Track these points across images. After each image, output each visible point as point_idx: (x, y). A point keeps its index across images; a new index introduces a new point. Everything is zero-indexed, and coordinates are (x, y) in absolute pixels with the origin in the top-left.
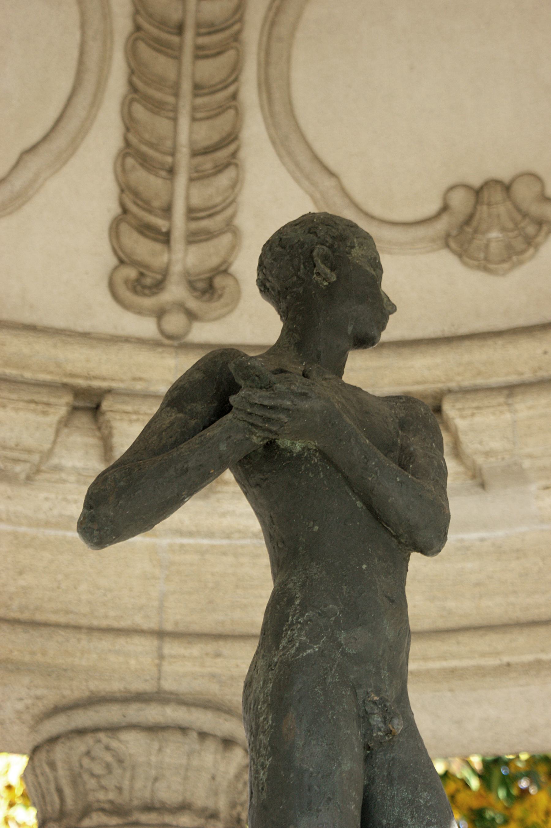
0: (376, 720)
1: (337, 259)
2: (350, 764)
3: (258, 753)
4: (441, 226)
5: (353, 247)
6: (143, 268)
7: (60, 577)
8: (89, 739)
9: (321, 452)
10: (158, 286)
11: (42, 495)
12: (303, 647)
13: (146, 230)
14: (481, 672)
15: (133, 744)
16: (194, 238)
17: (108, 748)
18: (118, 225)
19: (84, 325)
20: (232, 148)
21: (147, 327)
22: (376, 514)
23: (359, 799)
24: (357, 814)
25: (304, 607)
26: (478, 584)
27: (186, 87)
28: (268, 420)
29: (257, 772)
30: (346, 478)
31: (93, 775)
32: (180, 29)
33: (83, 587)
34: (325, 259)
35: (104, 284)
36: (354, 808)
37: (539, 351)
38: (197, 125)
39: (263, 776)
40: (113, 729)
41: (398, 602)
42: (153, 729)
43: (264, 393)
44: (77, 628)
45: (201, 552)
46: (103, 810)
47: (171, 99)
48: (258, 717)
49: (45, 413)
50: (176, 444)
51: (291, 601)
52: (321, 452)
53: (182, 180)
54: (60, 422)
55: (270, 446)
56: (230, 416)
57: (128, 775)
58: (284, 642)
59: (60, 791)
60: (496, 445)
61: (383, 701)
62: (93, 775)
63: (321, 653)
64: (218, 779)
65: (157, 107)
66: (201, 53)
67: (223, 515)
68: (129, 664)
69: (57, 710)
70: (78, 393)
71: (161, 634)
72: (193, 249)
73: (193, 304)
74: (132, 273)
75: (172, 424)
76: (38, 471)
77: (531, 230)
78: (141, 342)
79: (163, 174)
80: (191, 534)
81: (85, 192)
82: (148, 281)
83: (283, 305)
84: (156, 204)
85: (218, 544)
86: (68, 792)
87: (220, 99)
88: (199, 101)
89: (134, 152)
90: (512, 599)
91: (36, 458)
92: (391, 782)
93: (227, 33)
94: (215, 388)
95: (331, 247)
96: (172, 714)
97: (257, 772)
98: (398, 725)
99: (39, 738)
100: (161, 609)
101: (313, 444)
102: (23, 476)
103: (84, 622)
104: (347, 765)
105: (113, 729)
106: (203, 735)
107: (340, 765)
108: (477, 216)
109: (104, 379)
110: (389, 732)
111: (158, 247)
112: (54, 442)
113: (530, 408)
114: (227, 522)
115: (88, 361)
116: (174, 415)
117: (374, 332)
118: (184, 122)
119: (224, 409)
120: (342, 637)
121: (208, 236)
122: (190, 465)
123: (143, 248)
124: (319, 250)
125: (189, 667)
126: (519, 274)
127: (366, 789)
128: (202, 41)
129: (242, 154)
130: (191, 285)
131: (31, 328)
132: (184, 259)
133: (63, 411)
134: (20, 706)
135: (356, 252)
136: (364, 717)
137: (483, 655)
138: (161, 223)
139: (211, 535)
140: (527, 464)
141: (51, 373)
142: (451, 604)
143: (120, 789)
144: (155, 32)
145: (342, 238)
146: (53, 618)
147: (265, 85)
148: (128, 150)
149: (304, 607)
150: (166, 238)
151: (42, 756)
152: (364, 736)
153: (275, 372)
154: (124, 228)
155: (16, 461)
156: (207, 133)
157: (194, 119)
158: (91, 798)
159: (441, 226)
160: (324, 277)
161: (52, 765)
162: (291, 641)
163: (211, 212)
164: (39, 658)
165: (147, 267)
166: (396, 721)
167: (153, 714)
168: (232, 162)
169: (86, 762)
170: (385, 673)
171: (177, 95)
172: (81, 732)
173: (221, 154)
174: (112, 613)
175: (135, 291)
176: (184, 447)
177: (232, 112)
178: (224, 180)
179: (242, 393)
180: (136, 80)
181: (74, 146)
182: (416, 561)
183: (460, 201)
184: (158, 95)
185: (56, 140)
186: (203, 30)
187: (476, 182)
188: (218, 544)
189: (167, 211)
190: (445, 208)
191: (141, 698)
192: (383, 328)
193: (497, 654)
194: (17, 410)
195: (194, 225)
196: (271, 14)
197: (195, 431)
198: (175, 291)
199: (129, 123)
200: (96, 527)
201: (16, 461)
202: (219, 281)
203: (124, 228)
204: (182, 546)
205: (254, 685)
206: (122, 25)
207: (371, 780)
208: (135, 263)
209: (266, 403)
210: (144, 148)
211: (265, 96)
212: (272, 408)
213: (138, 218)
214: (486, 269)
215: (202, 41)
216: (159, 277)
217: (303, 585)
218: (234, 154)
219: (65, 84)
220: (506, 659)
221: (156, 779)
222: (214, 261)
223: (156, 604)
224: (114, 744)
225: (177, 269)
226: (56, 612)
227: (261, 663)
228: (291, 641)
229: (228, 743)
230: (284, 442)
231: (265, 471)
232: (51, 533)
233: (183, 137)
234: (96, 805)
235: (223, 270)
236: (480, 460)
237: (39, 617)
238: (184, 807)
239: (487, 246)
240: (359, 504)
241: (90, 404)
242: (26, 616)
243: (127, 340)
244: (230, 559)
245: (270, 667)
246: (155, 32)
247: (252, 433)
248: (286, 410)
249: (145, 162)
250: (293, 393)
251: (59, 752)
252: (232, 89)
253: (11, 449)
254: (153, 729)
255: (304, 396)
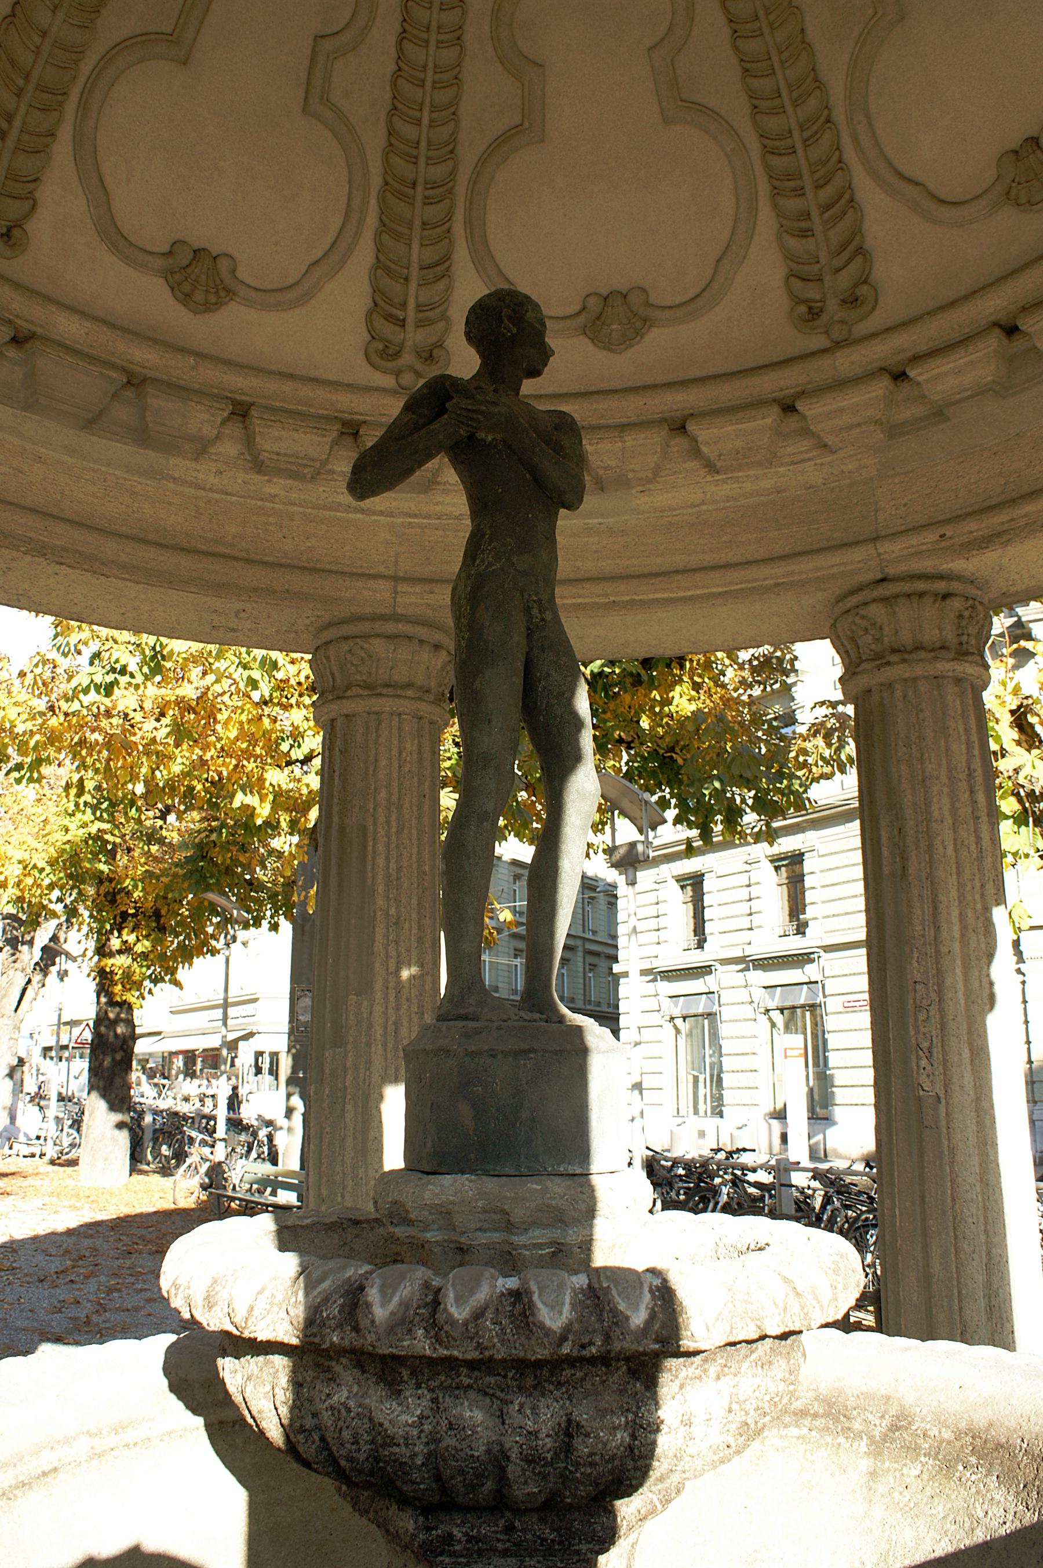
0: (535, 612)
1: (518, 319)
2: (518, 638)
3: (461, 631)
4: (581, 320)
5: (527, 311)
6: (387, 343)
7: (332, 541)
8: (351, 642)
9: (505, 441)
10: (397, 355)
11: (321, 489)
12: (490, 565)
13: (389, 318)
14: (597, 606)
15: (378, 646)
16: (420, 324)
17: (362, 648)
18: (400, 44)
19: (350, 379)
20: (447, 264)
21: (389, 381)
22: (539, 482)
23: (523, 659)
24: (522, 668)
25: (491, 540)
26: (596, 552)
27: (417, 223)
28: (471, 419)
29: (459, 641)
30: (520, 459)
31: (353, 665)
32: (414, 185)
33: (347, 548)
34: (510, 318)
35: (362, 353)
36: (520, 665)
37: (641, 403)
38: (423, 248)
39: (463, 644)
40: (366, 637)
41: (551, 540)
42: (389, 637)
43: (469, 401)
44: (344, 573)
45: (422, 527)
46: (359, 686)
47: (407, 232)
48: (460, 608)
49: (324, 436)
50: (411, 434)
51: (483, 535)
52: (505, 441)
53: (413, 285)
54: (333, 441)
55: (472, 437)
56: (446, 416)
57: (375, 664)
58: (478, 562)
59: (332, 674)
60: (612, 463)
61: (540, 600)
62: (353, 665)
63: (502, 569)
64: (431, 669)
65: (397, 236)
66: (427, 202)
67: (436, 504)
68: (376, 596)
69: (330, 625)
70: (345, 423)
71: (396, 579)
72: (420, 330)
73: (419, 367)
74: (381, 346)
75: (408, 421)
76: (319, 473)
77: (639, 324)
78: (385, 390)
79: (402, 281)
80: (415, 516)
81: (350, 292)
82: (390, 352)
83: (481, 348)
84: (396, 301)
85: (438, 506)
86: (337, 674)
87: (439, 231)
88: (426, 233)
89: (381, 267)
90: (618, 561)
91: (318, 464)
92: (543, 651)
93: (445, 188)
94: (435, 400)
95: (513, 310)
96: (402, 628)
97: (459, 641)
98: (548, 615)
99: (319, 642)
100: (396, 562)
101: (499, 436)
102: (309, 476)
103: (348, 570)
104: (516, 638)
105: (366, 637)
106: (421, 641)
107: (512, 638)
108: (604, 315)
109: (362, 415)
110: (543, 620)
111: (398, 329)
112: (329, 454)
113: (634, 440)
114: (438, 508)
115: (351, 402)
116: (410, 416)
117: (540, 367)
118: (416, 246)
119: (443, 411)
120: (515, 559)
121: (430, 322)
122: (420, 447)
123: (387, 330)
124: (506, 312)
125: (414, 599)
126: (629, 354)
127: (528, 654)
128: (427, 193)
129: (453, 269)
130: (418, 355)
131: (315, 380)
132: (414, 337)
133: (335, 434)
134: (307, 622)
135: (529, 314)
136: (528, 609)
137: (598, 596)
138: (400, 314)
139: (428, 517)
140: (630, 475)
141: (327, 409)
142: (579, 564)
143: (370, 674)
144: (397, 186)
145: (521, 305)
146: (328, 567)
147: (469, 224)
148: (378, 264)
149: (491, 540)
150: (402, 323)
151: (322, 652)
152: (527, 621)
153: (477, 388)
154: (375, 315)
155: (305, 466)
156: (430, 255)
157: (422, 245)
158: (351, 678)
159: (581, 320)
160: (508, 329)
161: (328, 658)
162: (482, 561)
163: (431, 307)
164: (319, 591)
165: (390, 342)
166: (547, 612)
167: (391, 628)
168: (446, 274)
169: (348, 656)
170: (541, 584)
171: (411, 229)
172: (346, 638)
173: (439, 269)
174: (365, 565)
175: (382, 358)
176: (416, 436)
177: (447, 240)
178: (441, 285)
179: (454, 401)
180: (384, 218)
181: (343, 262)
182: (563, 512)
183: (593, 303)
184: (399, 228)
185: (330, 259)
186: (429, 186)
187: (605, 293)
188: (438, 506)
189: (404, 305)
190: (584, 309)
191: (383, 618)
192: (546, 365)
193: (607, 595)
194: (305, 433)
195: (421, 315)
196: (474, 176)
197: (423, 426)
198: (408, 358)
199: (379, 247)
200: (358, 486)
201: (305, 466)
202: (435, 353)
203: (375, 315)
204: (410, 523)
205: (459, 588)
206: (376, 181)
207: (531, 649)
208: (382, 340)
209: (470, 407)
210: (389, 264)
211: (468, 231)
212: (474, 411)
213: (384, 310)
214: (609, 350)
215: (427, 193)
216: (398, 349)
217: (491, 527)
218: (448, 269)
219: (338, 220)
220: (612, 599)
221: (392, 668)
222: (434, 339)
223: (393, 559)
224: (366, 646)
225: (409, 343)
226: (329, 563)
227: (463, 575)
228: (482, 561)
229: (437, 647)
230: (481, 435)
231: (467, 453)
232: (327, 513)
233: (415, 257)
234: (355, 683)
235: (439, 345)
236: (601, 472)
237: (319, 566)
238: (409, 685)
239: (610, 334)
240: (528, 476)
241: (352, 430)
242: (311, 565)
243: (376, 389)
244: (441, 533)
245: (469, 577)
246: (397, 186)
247: (459, 428)
248: (482, 413)
249: (389, 272)
250: (487, 401)
251: (332, 651)
252: (447, 225)
253: (302, 458)
254: (389, 637)
255: (495, 404)
